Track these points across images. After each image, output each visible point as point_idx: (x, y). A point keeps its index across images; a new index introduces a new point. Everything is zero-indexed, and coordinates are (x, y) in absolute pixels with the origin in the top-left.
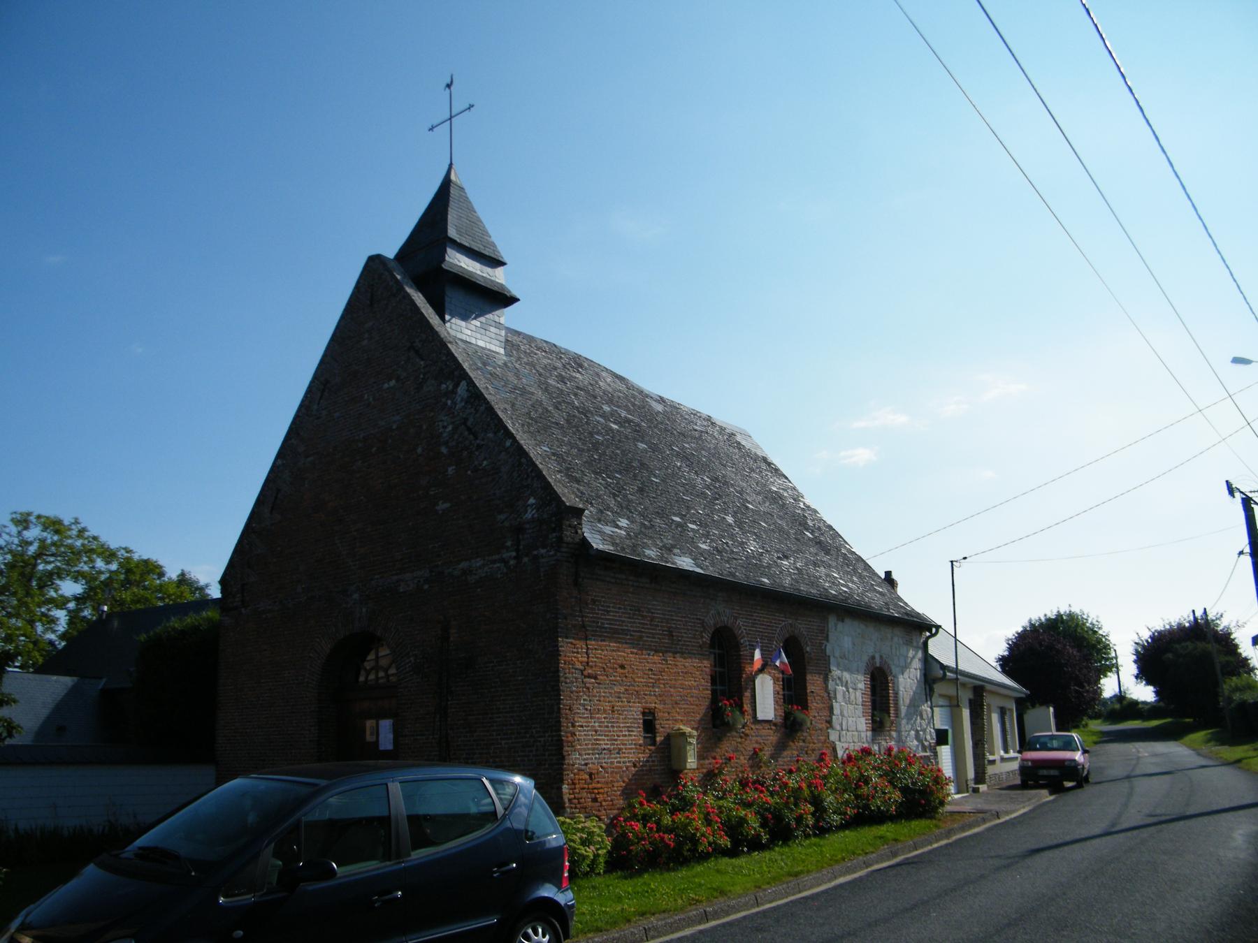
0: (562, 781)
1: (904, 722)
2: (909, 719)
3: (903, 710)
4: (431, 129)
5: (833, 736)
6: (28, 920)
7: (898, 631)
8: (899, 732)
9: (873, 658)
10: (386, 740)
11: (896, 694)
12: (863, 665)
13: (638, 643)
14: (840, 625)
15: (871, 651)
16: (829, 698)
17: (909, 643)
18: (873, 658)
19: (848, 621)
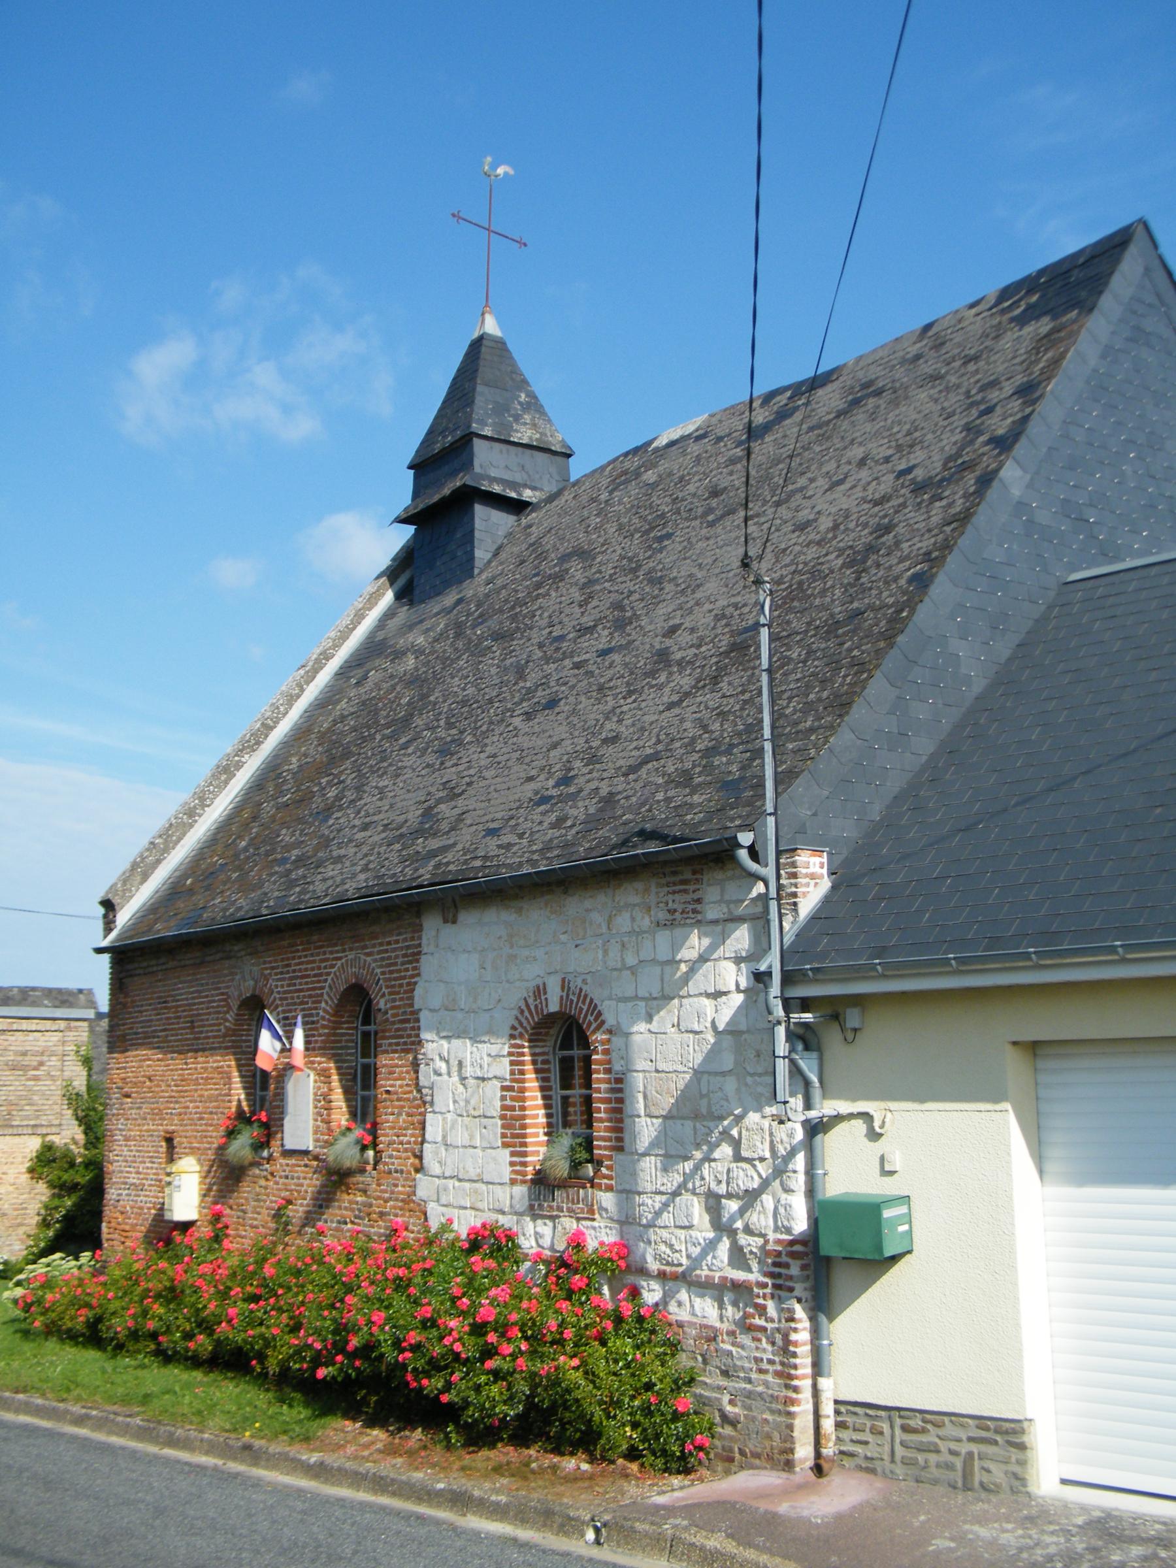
0: (101, 1222)
1: (649, 1167)
2: (670, 1159)
3: (646, 1130)
4: (169, 1141)
5: (425, 1187)
6: (788, 940)
7: (630, 894)
8: (628, 1193)
9: (540, 992)
10: (906, 1227)
11: (619, 1084)
12: (505, 1018)
13: (167, 1046)
14: (448, 931)
15: (533, 973)
16: (422, 1102)
17: (690, 915)
18: (540, 992)
19: (468, 918)
